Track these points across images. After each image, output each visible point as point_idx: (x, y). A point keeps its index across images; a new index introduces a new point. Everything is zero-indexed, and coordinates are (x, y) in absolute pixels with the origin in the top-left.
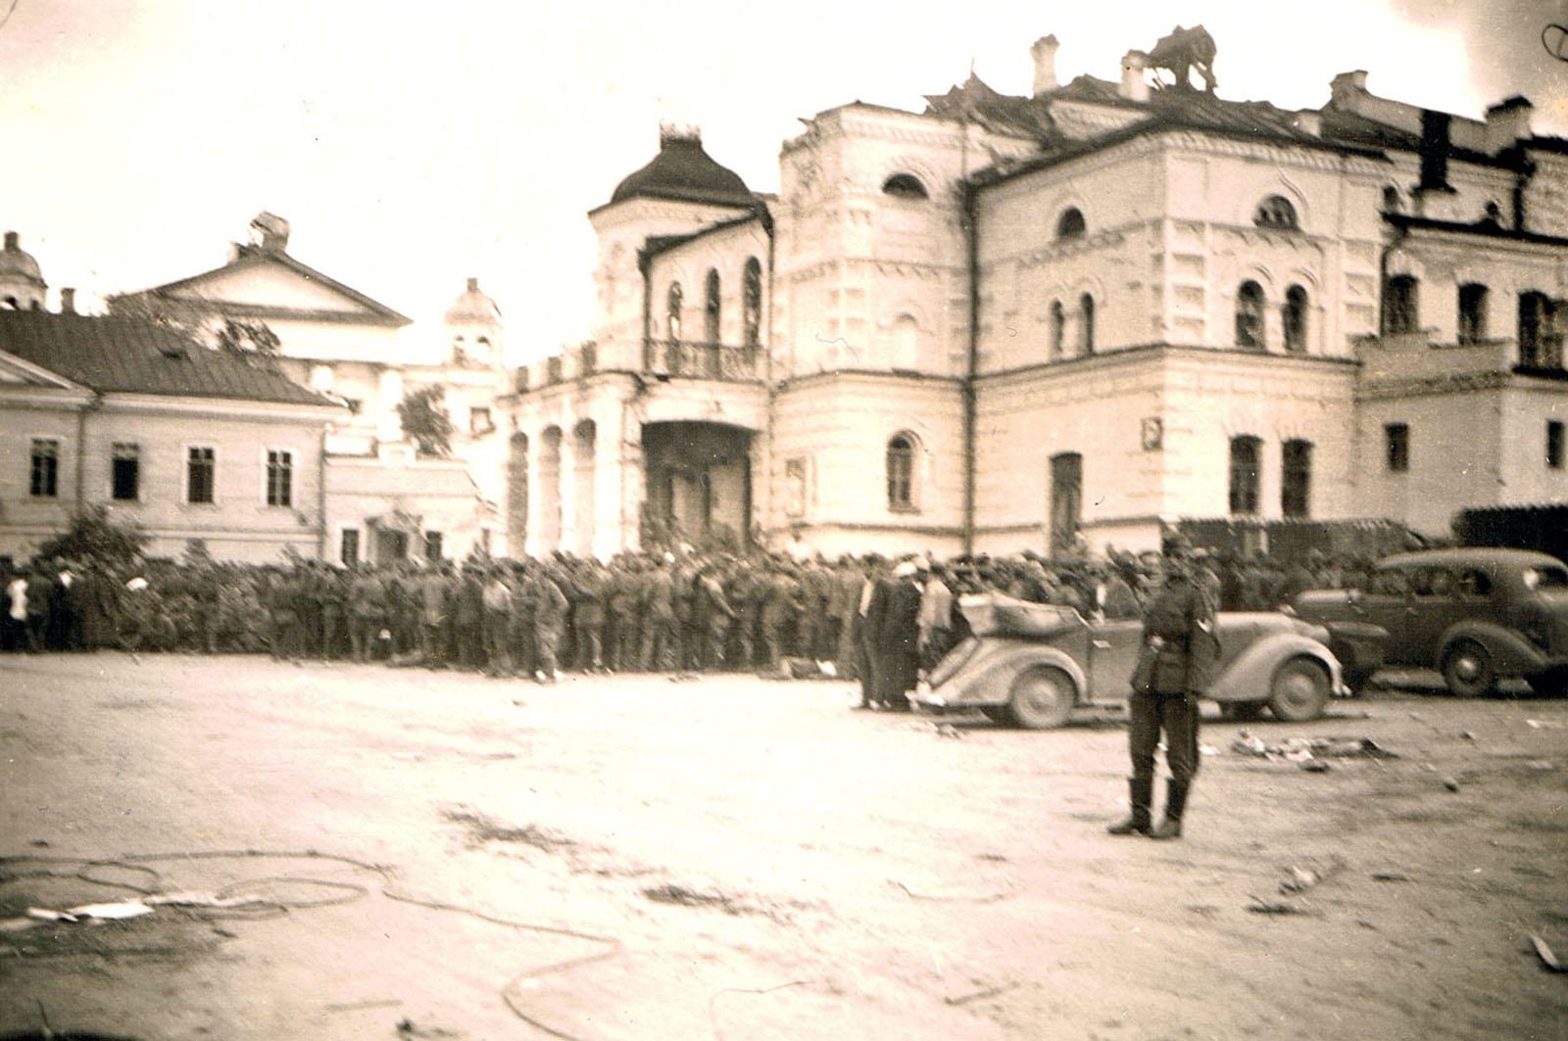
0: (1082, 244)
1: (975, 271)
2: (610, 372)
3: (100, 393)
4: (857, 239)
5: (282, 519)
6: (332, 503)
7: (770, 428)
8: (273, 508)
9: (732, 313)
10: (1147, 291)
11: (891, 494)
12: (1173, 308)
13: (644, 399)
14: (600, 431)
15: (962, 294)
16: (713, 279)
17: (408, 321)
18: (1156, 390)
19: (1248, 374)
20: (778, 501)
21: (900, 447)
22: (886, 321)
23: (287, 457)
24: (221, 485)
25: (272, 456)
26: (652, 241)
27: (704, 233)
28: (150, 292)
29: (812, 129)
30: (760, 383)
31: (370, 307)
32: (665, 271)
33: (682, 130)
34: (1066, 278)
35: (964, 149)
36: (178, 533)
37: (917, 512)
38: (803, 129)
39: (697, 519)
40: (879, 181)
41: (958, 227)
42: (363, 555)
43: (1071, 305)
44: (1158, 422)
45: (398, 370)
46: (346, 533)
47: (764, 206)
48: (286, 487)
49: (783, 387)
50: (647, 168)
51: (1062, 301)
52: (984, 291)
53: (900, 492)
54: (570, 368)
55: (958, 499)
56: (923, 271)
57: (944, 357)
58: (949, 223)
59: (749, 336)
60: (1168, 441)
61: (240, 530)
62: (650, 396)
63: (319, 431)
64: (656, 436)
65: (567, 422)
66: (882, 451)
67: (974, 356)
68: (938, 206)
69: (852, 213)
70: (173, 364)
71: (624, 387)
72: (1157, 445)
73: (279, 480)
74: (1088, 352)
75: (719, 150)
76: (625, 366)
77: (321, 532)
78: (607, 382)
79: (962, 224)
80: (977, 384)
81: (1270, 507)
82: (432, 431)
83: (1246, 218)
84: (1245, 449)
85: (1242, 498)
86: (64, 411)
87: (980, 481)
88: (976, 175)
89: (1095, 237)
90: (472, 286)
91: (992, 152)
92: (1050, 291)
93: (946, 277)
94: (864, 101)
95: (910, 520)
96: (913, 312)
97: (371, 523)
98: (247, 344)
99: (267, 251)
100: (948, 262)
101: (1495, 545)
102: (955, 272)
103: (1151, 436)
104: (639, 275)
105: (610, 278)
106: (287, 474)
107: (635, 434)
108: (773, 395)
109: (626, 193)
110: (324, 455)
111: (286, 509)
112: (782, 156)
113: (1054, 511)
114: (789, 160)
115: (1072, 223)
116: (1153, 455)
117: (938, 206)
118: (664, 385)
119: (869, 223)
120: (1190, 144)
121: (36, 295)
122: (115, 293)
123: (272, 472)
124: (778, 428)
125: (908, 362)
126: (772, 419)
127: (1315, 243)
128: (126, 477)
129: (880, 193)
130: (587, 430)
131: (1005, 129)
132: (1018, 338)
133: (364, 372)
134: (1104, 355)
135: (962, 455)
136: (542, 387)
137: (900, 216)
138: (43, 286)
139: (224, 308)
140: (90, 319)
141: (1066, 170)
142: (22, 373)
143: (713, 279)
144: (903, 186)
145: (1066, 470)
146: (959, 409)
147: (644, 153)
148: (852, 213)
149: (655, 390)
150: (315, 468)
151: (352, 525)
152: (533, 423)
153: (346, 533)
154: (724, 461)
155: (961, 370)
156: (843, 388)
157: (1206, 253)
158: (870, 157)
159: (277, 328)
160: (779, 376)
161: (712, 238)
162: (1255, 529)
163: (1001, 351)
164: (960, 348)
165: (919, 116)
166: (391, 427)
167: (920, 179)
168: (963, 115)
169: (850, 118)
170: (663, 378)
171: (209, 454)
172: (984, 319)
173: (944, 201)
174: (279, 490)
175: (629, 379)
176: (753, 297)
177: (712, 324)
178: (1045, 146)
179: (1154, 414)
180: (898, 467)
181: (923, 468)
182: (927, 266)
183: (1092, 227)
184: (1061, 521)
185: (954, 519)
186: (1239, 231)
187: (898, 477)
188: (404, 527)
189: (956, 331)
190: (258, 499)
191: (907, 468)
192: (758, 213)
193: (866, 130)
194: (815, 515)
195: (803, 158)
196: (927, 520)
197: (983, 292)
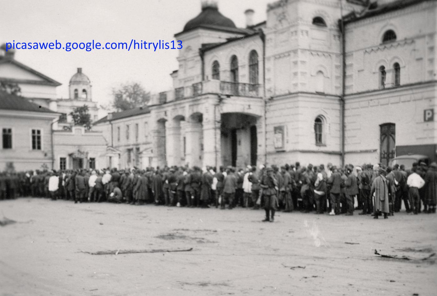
0: (395, 44)
1: (344, 54)
4: (303, 41)
5: (38, 154)
6: (56, 148)
7: (265, 115)
8: (35, 150)
10: (426, 61)
11: (317, 140)
13: (221, 105)
14: (205, 117)
15: (340, 63)
16: (234, 59)
18: (430, 99)
20: (269, 142)
21: (318, 121)
22: (314, 73)
23: (39, 132)
24: (15, 141)
25: (33, 132)
30: (261, 98)
32: (210, 58)
34: (388, 56)
37: (325, 146)
39: (229, 150)
40: (310, 20)
41: (337, 38)
42: (68, 167)
43: (389, 67)
46: (61, 159)
48: (39, 143)
49: (271, 99)
52: (348, 62)
53: (319, 139)
54: (188, 93)
56: (326, 54)
57: (334, 88)
58: (335, 36)
61: (23, 159)
62: (223, 103)
63: (51, 122)
64: (226, 117)
65: (187, 113)
66: (313, 123)
67: (344, 87)
68: (331, 30)
69: (302, 31)
71: (213, 100)
73: (36, 140)
74: (397, 85)
76: (214, 92)
77: (53, 159)
78: (208, 98)
79: (339, 37)
80: (345, 98)
87: (347, 134)
89: (401, 41)
90: (79, 71)
93: (334, 57)
95: (322, 149)
97: (70, 155)
100: (335, 51)
101: (413, 154)
102: (337, 55)
104: (199, 58)
106: (39, 138)
108: (266, 103)
109: (191, 27)
110: (52, 131)
111: (39, 151)
112: (268, 11)
113: (381, 145)
114: (272, 12)
115: (389, 36)
116: (430, 124)
117: (331, 30)
118: (228, 99)
123: (34, 137)
125: (321, 90)
126: (266, 112)
130: (198, 118)
132: (364, 78)
135: (340, 124)
137: (317, 33)
143: (234, 59)
145: (387, 130)
147: (195, 12)
148: (302, 31)
149: (224, 101)
150: (49, 135)
151: (63, 156)
153: (61, 159)
154: (243, 128)
155: (339, 92)
156: (300, 99)
160: (268, 95)
163: (355, 84)
164: (339, 83)
170: (228, 96)
171: (10, 130)
172: (348, 73)
173: (333, 27)
174: (36, 143)
175: (216, 96)
177: (233, 76)
179: (431, 108)
180: (318, 130)
182: (327, 52)
183: (400, 36)
184: (385, 148)
185: (337, 149)
187: (318, 133)
188: (82, 156)
189: (337, 77)
190: (29, 147)
191: (320, 130)
194: (288, 148)
195: (279, 11)
196: (328, 149)
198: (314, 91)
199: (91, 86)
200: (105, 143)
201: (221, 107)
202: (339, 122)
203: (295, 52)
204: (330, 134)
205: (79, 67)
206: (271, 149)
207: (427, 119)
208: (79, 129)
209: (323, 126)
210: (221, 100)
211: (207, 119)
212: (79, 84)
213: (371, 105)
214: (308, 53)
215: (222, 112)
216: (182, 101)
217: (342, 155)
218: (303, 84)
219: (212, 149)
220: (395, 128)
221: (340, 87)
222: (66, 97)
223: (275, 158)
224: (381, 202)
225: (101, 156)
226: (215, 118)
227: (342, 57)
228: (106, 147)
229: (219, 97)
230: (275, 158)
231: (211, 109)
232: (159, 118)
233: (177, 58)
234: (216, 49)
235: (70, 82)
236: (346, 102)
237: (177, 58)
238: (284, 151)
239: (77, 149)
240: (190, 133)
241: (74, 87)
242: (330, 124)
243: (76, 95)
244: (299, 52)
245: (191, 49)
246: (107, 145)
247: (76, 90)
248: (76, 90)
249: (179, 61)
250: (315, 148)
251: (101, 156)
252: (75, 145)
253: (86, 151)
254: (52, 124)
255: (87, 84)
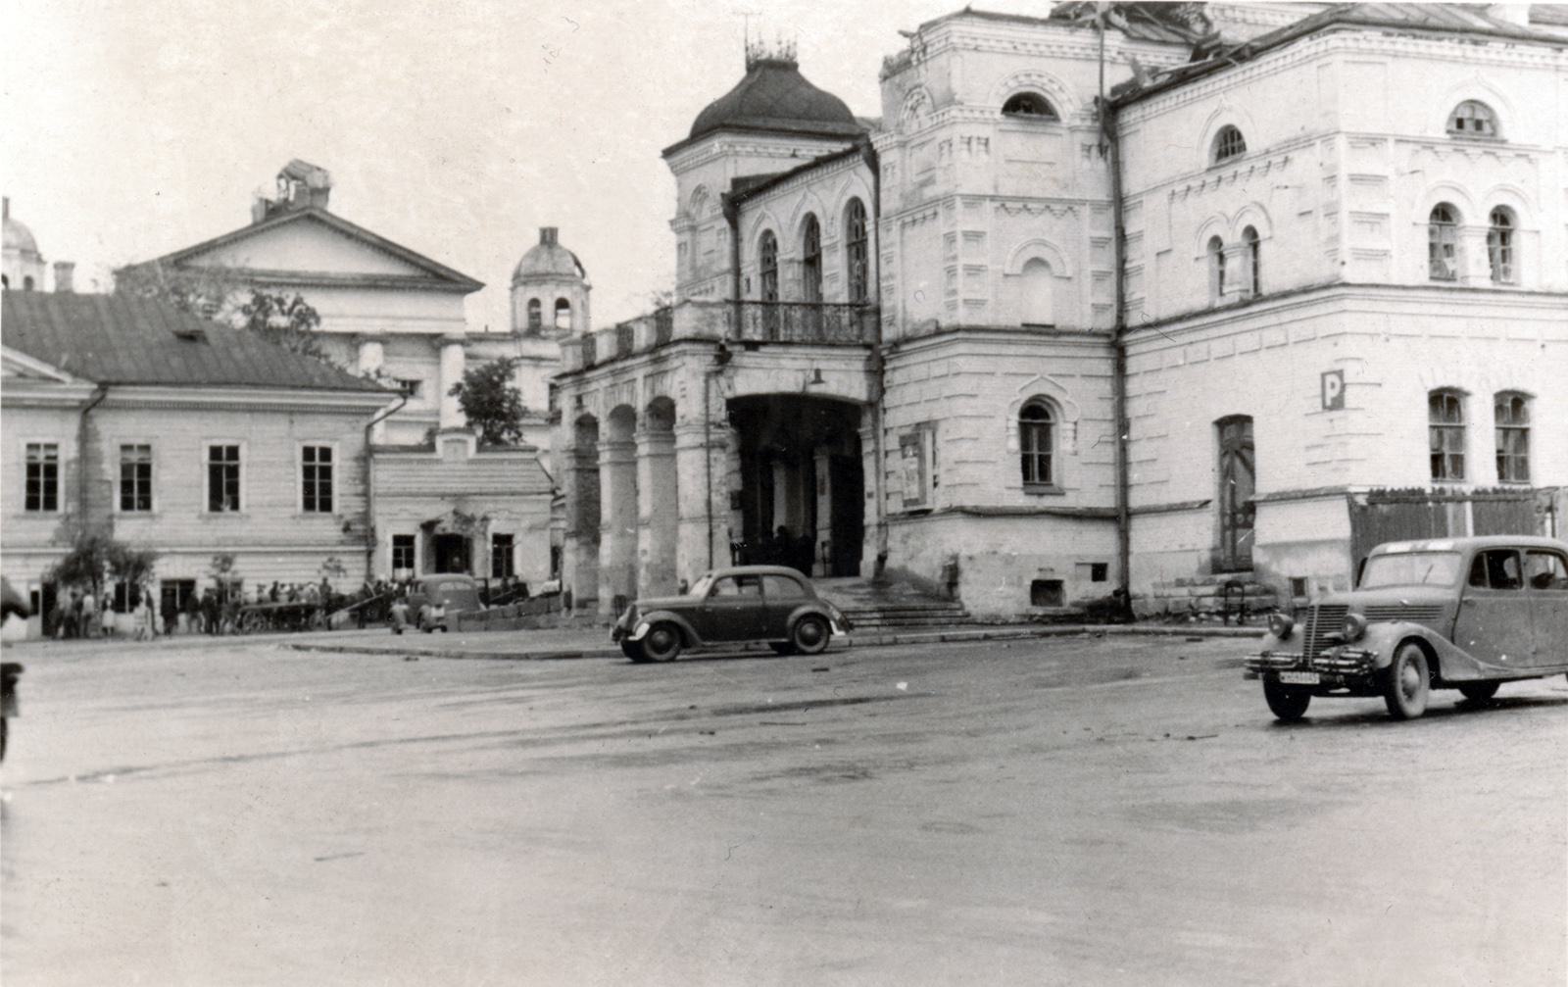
0: (1243, 168)
2: (687, 340)
3: (104, 386)
5: (324, 528)
9: (835, 263)
12: (1353, 238)
13: (729, 372)
15: (1108, 232)
16: (811, 225)
17: (476, 286)
19: (1439, 315)
21: (1036, 417)
23: (326, 454)
25: (308, 453)
26: (737, 182)
27: (798, 171)
28: (162, 261)
29: (917, 44)
31: (423, 268)
32: (759, 217)
33: (772, 50)
35: (1102, 61)
36: (438, 473)
37: (1061, 493)
38: (904, 44)
43: (1233, 237)
44: (1340, 374)
45: (462, 343)
47: (864, 135)
48: (327, 489)
50: (730, 95)
51: (1221, 234)
53: (1036, 467)
55: (1109, 475)
59: (855, 291)
60: (1351, 397)
63: (364, 422)
65: (641, 402)
70: (188, 347)
72: (1338, 404)
75: (819, 73)
77: (369, 539)
80: (1127, 338)
81: (1481, 472)
82: (502, 416)
83: (1437, 126)
84: (1446, 402)
85: (1447, 463)
86: (63, 408)
88: (1115, 91)
90: (549, 237)
91: (1134, 64)
92: (1207, 224)
94: (975, 7)
95: (1048, 502)
96: (1044, 254)
97: (428, 527)
98: (279, 320)
99: (299, 206)
102: (1098, 208)
103: (1331, 394)
104: (724, 223)
105: (693, 229)
106: (326, 473)
107: (720, 413)
109: (708, 125)
115: (1230, 143)
116: (1335, 414)
119: (987, 151)
120: (1364, 45)
121: (32, 270)
122: (123, 263)
123: (308, 472)
124: (889, 399)
127: (1523, 154)
128: (137, 488)
129: (998, 115)
130: (663, 411)
131: (1147, 33)
133: (422, 348)
134: (1273, 297)
136: (612, 361)
137: (1018, 141)
138: (40, 260)
139: (251, 279)
140: (90, 300)
141: (1220, 80)
142: (11, 365)
143: (811, 225)
144: (1026, 106)
145: (1235, 435)
146: (1106, 367)
147: (726, 78)
151: (405, 530)
152: (599, 406)
155: (1107, 322)
156: (1348, 304)
157: (1388, 171)
158: (984, 78)
159: (314, 300)
161: (808, 177)
162: (1459, 499)
165: (1043, 22)
166: (453, 415)
167: (1048, 97)
168: (1099, 21)
169: (961, 29)
174: (317, 493)
176: (857, 246)
178: (1198, 53)
181: (1063, 444)
182: (1060, 201)
183: (1253, 141)
185: (1106, 500)
186: (1429, 145)
190: (294, 505)
191: (1045, 441)
192: (854, 142)
193: (984, 45)
194: (938, 501)
197: (1130, 230)
198: (1017, 323)
199: (588, 288)
200: (546, 485)
201: (731, 378)
202: (1110, 416)
203: (1327, 138)
204: (1076, 453)
205: (547, 224)
206: (895, 506)
207: (1329, 403)
208: (459, 441)
209: (1053, 430)
210: (723, 358)
211: (683, 417)
212: (544, 282)
213: (1191, 359)
214: (989, 206)
215: (729, 394)
216: (628, 363)
217: (1120, 518)
218: (975, 304)
219: (700, 508)
220: (598, 480)
221: (1111, 306)
222: (503, 326)
223: (908, 536)
224: (679, 657)
225: (532, 529)
226: (707, 415)
227: (1111, 213)
228: (550, 497)
229: (722, 348)
230: (908, 536)
231: (696, 387)
232: (612, 406)
233: (672, 222)
234: (777, 192)
235: (517, 276)
236: (1130, 351)
237: (672, 222)
238: (926, 512)
239: (452, 507)
240: (648, 460)
241: (532, 292)
242: (1076, 423)
243: (535, 317)
244: (1341, 142)
245: (706, 196)
246: (553, 492)
247: (535, 303)
248: (535, 303)
249: (679, 232)
250: (1021, 500)
251: (532, 529)
252: (443, 496)
253: (479, 514)
254: (369, 428)
255: (571, 283)
